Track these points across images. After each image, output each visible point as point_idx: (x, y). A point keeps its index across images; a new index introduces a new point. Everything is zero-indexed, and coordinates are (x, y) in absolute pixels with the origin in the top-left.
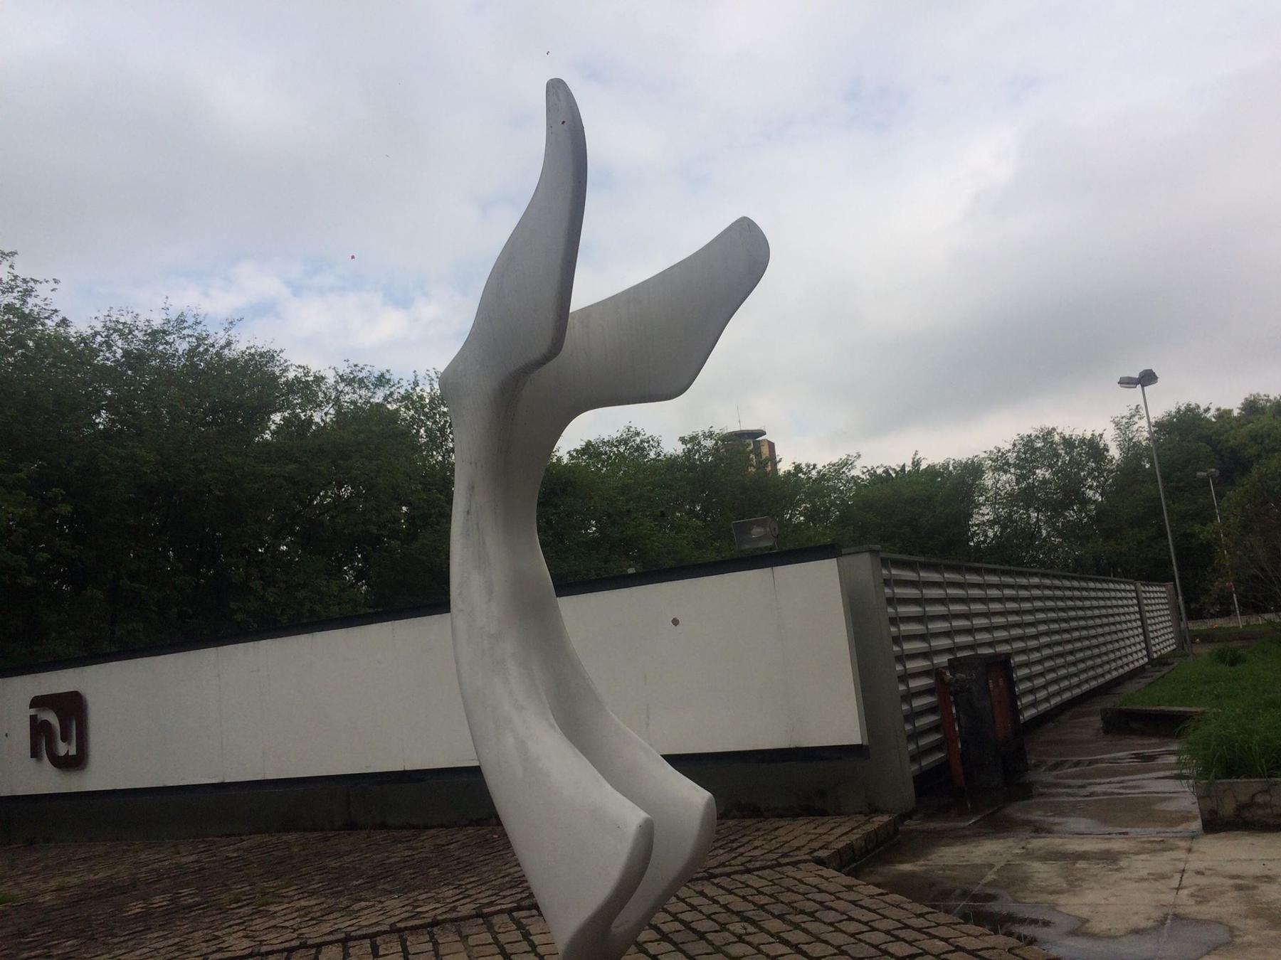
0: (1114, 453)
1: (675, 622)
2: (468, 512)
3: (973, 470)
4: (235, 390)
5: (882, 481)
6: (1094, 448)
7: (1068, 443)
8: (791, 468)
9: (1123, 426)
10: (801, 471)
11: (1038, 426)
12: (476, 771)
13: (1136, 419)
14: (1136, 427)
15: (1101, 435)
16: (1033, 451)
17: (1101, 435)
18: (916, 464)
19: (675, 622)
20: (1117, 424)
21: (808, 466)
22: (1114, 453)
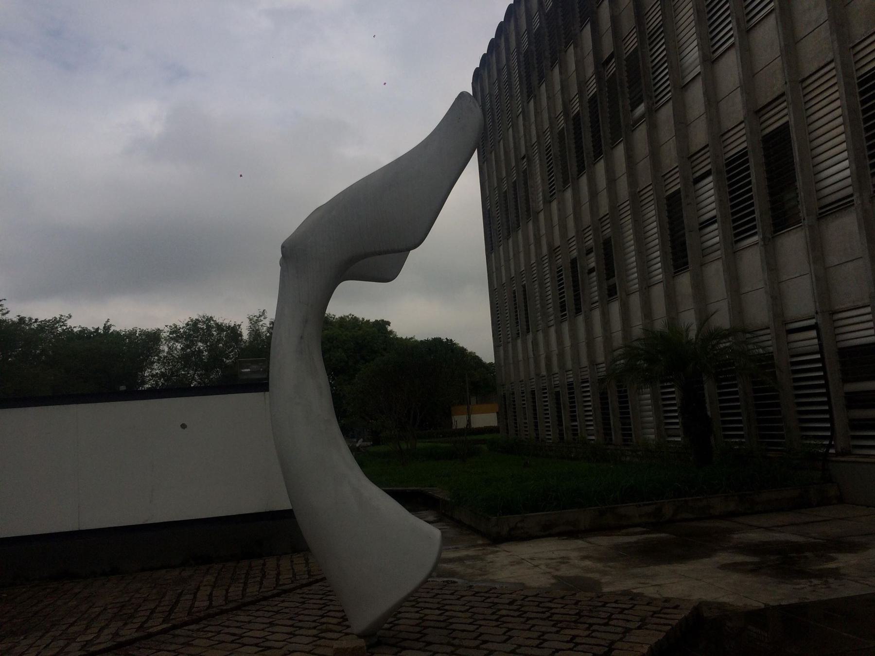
0: (245, 335)
1: (184, 426)
2: (302, 338)
3: (154, 337)
4: (355, 319)
5: (84, 335)
6: (233, 332)
7: (220, 327)
8: (16, 319)
9: (254, 322)
10: (24, 322)
11: (201, 315)
12: (287, 515)
13: (262, 318)
14: (261, 323)
15: (239, 326)
16: (198, 331)
17: (239, 326)
18: (107, 328)
19: (184, 426)
20: (251, 320)
21: (30, 319)
22: (245, 335)
